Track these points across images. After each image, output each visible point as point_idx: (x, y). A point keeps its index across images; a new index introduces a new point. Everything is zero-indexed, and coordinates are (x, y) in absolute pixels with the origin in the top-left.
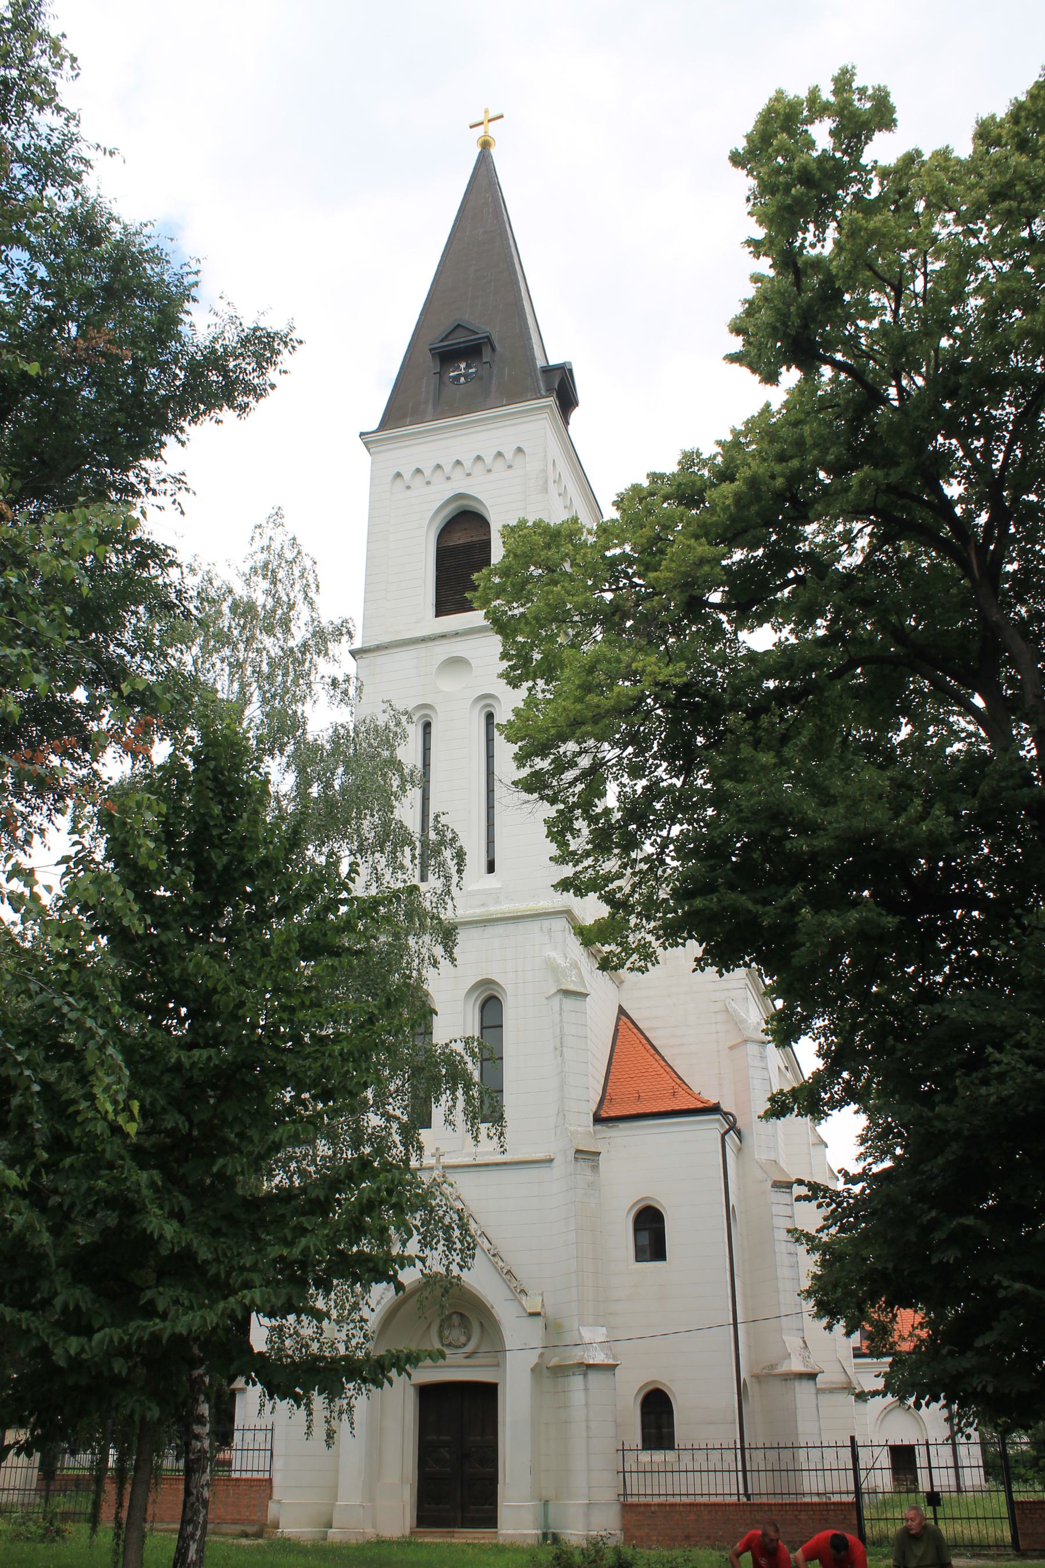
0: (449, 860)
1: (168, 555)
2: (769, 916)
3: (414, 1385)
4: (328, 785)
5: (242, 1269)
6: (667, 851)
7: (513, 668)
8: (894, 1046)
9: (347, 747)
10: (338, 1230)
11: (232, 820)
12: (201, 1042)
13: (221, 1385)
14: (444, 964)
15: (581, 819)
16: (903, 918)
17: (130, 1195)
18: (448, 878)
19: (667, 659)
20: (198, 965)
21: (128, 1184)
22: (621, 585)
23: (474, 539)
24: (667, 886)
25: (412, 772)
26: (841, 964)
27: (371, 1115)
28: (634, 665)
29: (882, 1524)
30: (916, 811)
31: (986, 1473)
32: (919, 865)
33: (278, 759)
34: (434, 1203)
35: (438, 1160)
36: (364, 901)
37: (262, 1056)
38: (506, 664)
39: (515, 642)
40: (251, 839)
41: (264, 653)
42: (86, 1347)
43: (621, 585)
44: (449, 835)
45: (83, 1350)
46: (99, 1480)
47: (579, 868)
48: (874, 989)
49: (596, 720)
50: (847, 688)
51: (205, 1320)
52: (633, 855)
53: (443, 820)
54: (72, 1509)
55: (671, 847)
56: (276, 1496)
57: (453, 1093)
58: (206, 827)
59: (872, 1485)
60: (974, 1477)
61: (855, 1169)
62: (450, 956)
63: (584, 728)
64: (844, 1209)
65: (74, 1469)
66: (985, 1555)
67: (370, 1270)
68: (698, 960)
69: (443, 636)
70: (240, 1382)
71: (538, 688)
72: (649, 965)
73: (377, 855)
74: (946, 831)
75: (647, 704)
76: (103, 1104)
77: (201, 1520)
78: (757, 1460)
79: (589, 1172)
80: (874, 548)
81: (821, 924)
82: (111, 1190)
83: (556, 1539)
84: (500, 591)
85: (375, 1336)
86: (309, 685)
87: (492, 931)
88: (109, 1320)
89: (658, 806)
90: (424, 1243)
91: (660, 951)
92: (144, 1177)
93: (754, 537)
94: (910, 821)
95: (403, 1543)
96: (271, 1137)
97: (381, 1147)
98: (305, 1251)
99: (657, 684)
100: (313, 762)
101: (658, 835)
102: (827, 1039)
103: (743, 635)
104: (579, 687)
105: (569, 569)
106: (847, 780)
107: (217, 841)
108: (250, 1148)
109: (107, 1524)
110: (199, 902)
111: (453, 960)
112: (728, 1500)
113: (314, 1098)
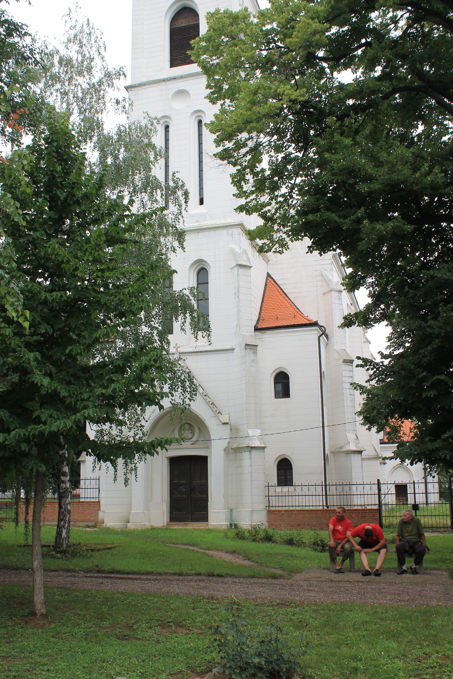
0: (180, 196)
1: (23, 29)
2: (346, 224)
3: (167, 458)
4: (116, 158)
5: (83, 400)
6: (294, 191)
7: (213, 93)
8: (408, 291)
9: (126, 137)
10: (130, 380)
11: (67, 174)
12: (57, 288)
13: (73, 458)
14: (179, 250)
15: (249, 174)
16: (416, 226)
17: (25, 365)
18: (180, 206)
19: (296, 87)
20: (53, 249)
21: (24, 359)
22: (271, 47)
23: (191, 23)
24: (294, 209)
25: (160, 150)
26: (382, 250)
27: (143, 327)
28: (278, 90)
29: (391, 518)
30: (425, 170)
31: (440, 496)
32: (424, 200)
33: (89, 144)
34: (176, 369)
35: (177, 350)
36: (138, 215)
37: (88, 295)
38: (209, 91)
39: (214, 79)
40: (78, 183)
41: (79, 86)
42: (8, 438)
43: (271, 47)
44: (180, 183)
45: (6, 440)
46: (17, 503)
47: (248, 200)
48: (399, 264)
49: (258, 120)
50: (390, 105)
51: (66, 424)
52: (276, 193)
53: (177, 175)
54: (5, 516)
55: (296, 189)
56: (102, 509)
57: (184, 315)
58: (54, 177)
59: (387, 501)
60: (434, 498)
61: (387, 352)
62: (182, 247)
63: (252, 125)
64: (380, 371)
65: (4, 499)
66: (438, 531)
67: (146, 400)
68: (309, 247)
69: (175, 78)
70: (83, 456)
71: (226, 104)
72: (284, 250)
73: (143, 194)
74: (440, 181)
75: (284, 113)
76: (11, 313)
77: (67, 519)
78: (332, 490)
79: (252, 355)
80: (409, 26)
81: (373, 229)
82: (15, 363)
83: (236, 526)
84: (206, 50)
85: (148, 434)
86: (104, 104)
87: (202, 235)
88: (18, 426)
89: (289, 167)
90: (172, 388)
91: (289, 243)
92: (31, 356)
93: (344, 19)
94: (421, 175)
95: (163, 529)
96: (95, 335)
97: (150, 341)
98: (114, 390)
99: (291, 101)
100: (108, 145)
101: (289, 183)
102: (373, 288)
103: (335, 74)
104: (249, 102)
105: (243, 38)
106: (389, 154)
107: (60, 185)
108: (84, 341)
109: (22, 523)
110: (52, 216)
111: (183, 248)
112: (318, 508)
113: (115, 316)
